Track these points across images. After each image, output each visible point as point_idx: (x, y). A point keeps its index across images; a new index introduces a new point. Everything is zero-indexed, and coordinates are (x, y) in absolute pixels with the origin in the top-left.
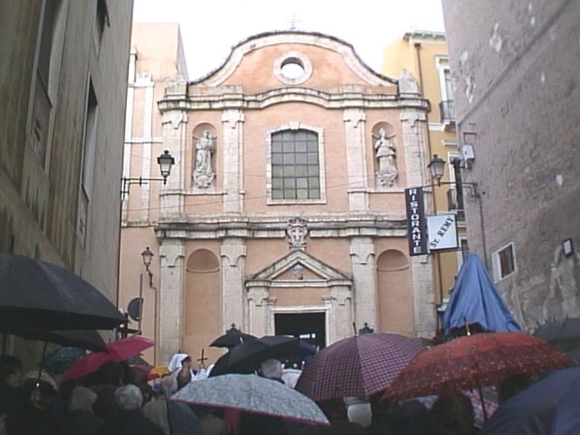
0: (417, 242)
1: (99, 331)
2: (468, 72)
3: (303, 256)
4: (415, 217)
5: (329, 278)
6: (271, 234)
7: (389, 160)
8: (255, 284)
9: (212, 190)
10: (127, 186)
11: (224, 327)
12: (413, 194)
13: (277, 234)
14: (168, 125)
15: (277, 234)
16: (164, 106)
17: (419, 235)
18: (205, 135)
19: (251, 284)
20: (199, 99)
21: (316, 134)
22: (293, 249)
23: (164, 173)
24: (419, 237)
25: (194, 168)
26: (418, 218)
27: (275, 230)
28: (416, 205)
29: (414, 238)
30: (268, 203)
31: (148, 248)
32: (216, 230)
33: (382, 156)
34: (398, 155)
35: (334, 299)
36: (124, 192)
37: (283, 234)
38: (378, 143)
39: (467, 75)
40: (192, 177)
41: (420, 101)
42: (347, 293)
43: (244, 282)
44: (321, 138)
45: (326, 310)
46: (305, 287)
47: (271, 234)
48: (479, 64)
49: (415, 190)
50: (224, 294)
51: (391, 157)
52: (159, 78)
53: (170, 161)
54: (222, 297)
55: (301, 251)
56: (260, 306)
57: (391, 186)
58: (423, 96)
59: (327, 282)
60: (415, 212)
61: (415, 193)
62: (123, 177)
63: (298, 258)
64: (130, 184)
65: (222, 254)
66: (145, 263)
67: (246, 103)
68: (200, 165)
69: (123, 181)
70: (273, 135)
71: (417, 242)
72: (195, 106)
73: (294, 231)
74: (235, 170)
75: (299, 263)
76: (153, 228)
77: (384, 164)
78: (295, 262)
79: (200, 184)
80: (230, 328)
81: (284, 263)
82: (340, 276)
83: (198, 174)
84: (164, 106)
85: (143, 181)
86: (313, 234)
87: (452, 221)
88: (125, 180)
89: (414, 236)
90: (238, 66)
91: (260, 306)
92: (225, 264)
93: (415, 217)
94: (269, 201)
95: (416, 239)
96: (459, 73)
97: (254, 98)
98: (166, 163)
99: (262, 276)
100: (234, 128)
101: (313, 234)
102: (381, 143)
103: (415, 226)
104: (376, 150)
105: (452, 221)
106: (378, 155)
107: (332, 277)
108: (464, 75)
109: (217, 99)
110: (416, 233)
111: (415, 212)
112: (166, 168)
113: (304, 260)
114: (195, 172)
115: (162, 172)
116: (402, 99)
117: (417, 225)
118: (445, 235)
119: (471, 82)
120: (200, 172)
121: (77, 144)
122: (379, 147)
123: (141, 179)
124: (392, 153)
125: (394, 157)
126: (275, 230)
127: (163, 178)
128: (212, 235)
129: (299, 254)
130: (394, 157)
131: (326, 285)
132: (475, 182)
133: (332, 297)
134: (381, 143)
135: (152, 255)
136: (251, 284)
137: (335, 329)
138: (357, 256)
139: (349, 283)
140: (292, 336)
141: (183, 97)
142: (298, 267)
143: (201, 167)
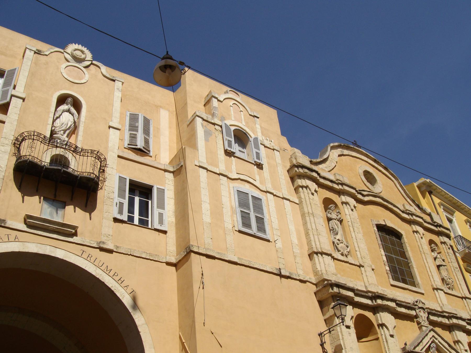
128: (368, 302)
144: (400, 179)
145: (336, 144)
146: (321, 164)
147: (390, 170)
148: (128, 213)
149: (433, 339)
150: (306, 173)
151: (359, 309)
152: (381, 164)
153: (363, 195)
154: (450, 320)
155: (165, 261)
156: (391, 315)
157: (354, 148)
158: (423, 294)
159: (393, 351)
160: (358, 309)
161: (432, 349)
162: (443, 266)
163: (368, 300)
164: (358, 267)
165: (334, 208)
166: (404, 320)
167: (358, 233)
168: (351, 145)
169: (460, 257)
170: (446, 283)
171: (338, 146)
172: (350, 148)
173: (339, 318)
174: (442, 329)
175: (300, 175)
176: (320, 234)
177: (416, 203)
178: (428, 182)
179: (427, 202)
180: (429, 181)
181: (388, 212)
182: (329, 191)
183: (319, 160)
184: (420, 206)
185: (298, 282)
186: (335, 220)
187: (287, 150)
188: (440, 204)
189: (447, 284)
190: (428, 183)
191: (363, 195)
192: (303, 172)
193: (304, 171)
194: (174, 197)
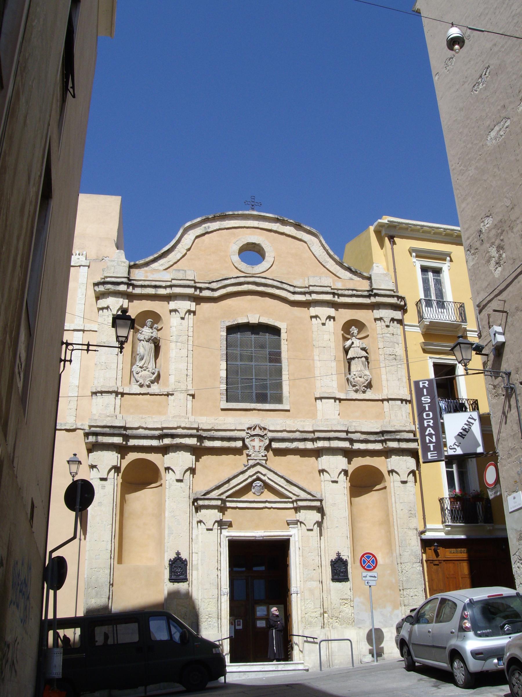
0: (431, 445)
1: (189, 471)
2: (493, 240)
3: (264, 471)
4: (428, 415)
5: (294, 498)
9: (155, 388)
10: (69, 352)
12: (424, 387)
16: (101, 288)
17: (434, 437)
20: (143, 283)
22: (251, 463)
23: (121, 339)
24: (434, 440)
25: (132, 364)
27: (230, 439)
29: (428, 441)
31: (75, 455)
33: (353, 358)
34: (372, 358)
36: (65, 361)
37: (239, 444)
38: (348, 343)
39: (493, 243)
40: (131, 372)
41: (396, 298)
43: (192, 500)
44: (283, 335)
45: (291, 536)
46: (266, 508)
47: (226, 444)
48: (511, 228)
49: (427, 383)
50: (167, 514)
51: (364, 359)
52: (95, 257)
53: (129, 322)
56: (211, 530)
57: (364, 392)
59: (292, 502)
60: (427, 409)
61: (426, 385)
62: (65, 341)
63: (258, 472)
64: (73, 350)
67: (198, 290)
68: (142, 359)
69: (64, 346)
70: (231, 330)
71: (431, 445)
72: (138, 291)
74: (183, 366)
75: (258, 479)
76: (81, 432)
78: (255, 477)
79: (141, 381)
80: (173, 556)
81: (241, 478)
82: (309, 497)
84: (101, 288)
86: (275, 445)
87: (475, 420)
88: (68, 344)
89: (427, 438)
90: (189, 250)
91: (211, 530)
92: (168, 478)
93: (428, 415)
94: (224, 405)
95: (431, 442)
96: (478, 244)
97: (207, 285)
98: (123, 326)
99: (214, 494)
100: (183, 318)
101: (275, 445)
102: (353, 343)
103: (429, 426)
104: (346, 351)
105: (475, 420)
106: (348, 357)
107: (298, 496)
108: (487, 245)
109: (164, 284)
110: (430, 435)
111: (427, 409)
112: (123, 332)
113: (264, 475)
114: (135, 366)
115: (117, 337)
116: (376, 295)
118: (465, 439)
119: (498, 251)
120: (141, 367)
121: (28, 219)
122: (350, 347)
123: (88, 350)
124: (364, 353)
125: (367, 358)
126: (230, 439)
127: (117, 344)
128: (155, 443)
130: (367, 358)
131: (290, 505)
132: (508, 371)
133: (298, 521)
134: (353, 343)
135: (80, 463)
136: (201, 503)
139: (318, 504)
142: (258, 483)
143: (143, 362)
144: (322, 235)
145: (199, 219)
146: (157, 262)
147: (304, 227)
149: (430, 431)
151: (139, 453)
152: (288, 222)
153: (213, 290)
154: (315, 443)
157: (234, 214)
159: (174, 499)
160: (138, 453)
161: (254, 488)
162: (356, 359)
163: (154, 440)
164: (166, 396)
165: (149, 323)
166: (221, 455)
168: (227, 211)
169: (421, 332)
170: (351, 384)
171: (204, 221)
172: (227, 216)
173: (461, 364)
175: (105, 293)
176: (107, 368)
177: (345, 266)
179: (384, 253)
180: (388, 221)
181: (267, 300)
182: (151, 301)
183: (142, 262)
184: (352, 268)
185: (64, 431)
186: (144, 341)
187: (108, 257)
188: (411, 251)
189: (354, 386)
191: (213, 290)
194: (66, 313)
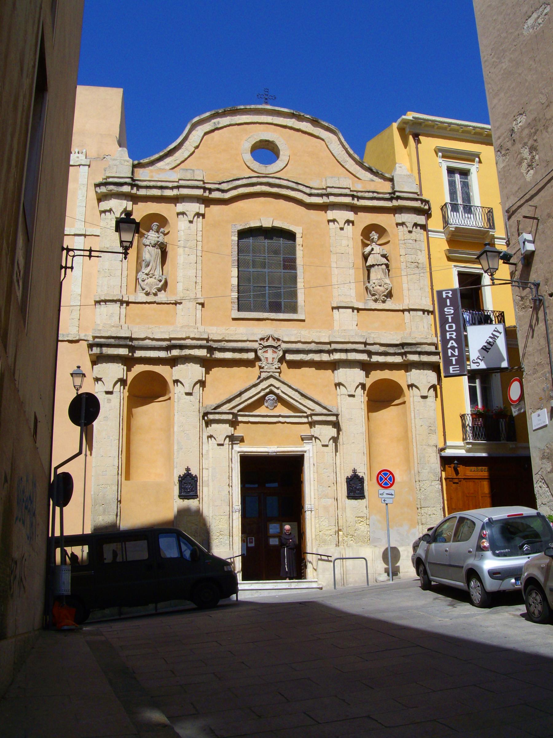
0: (454, 359)
3: (277, 384)
4: (451, 327)
5: (309, 412)
6: (237, 356)
7: (382, 269)
8: (217, 417)
9: (162, 297)
10: (70, 259)
11: (175, 470)
13: (245, 356)
14: (107, 214)
15: (245, 356)
16: (103, 189)
17: (456, 350)
18: (155, 228)
19: (211, 417)
21: (290, 236)
24: (456, 354)
26: (454, 328)
28: (452, 311)
30: (234, 316)
31: (79, 367)
32: (168, 348)
33: (373, 266)
34: (392, 266)
35: (316, 438)
36: (66, 268)
37: (251, 355)
38: (368, 249)
39: (525, 144)
40: (137, 279)
41: (419, 202)
42: (333, 432)
43: (202, 414)
44: (299, 240)
45: (305, 452)
46: (280, 422)
47: (237, 356)
49: (451, 293)
51: (384, 267)
54: (174, 432)
55: (275, 378)
56: (222, 445)
57: (384, 302)
58: (422, 195)
59: (307, 417)
60: (450, 320)
61: (450, 295)
63: (271, 385)
64: (74, 256)
65: (174, 378)
66: (75, 386)
67: (207, 192)
70: (243, 234)
72: (142, 192)
73: (266, 352)
75: (271, 392)
76: (85, 343)
77: (376, 274)
78: (268, 390)
79: (147, 289)
80: (183, 472)
82: (325, 411)
83: (145, 277)
84: (103, 189)
85: (87, 253)
86: (289, 357)
87: (500, 333)
88: (68, 250)
89: (450, 351)
90: (197, 147)
91: (222, 445)
92: (177, 392)
93: (451, 327)
94: (236, 314)
95: (453, 355)
96: (509, 144)
97: (217, 186)
100: (191, 222)
101: (289, 357)
103: (451, 338)
104: (366, 258)
105: (500, 333)
106: (368, 264)
108: (519, 146)
109: (170, 185)
110: (453, 348)
111: (450, 320)
112: (127, 237)
113: (278, 388)
115: (121, 242)
116: (398, 198)
117: (454, 336)
120: (147, 274)
123: (90, 256)
124: (384, 261)
125: (387, 266)
127: (121, 250)
128: (162, 354)
129: (272, 381)
130: (387, 266)
131: (305, 420)
132: (537, 282)
133: (313, 436)
134: (372, 249)
135: (84, 375)
136: (211, 417)
137: (316, 476)
138: (343, 385)
139: (333, 418)
140: (276, 485)
141: (128, 180)
145: (208, 114)
148: (182, 497)
150: (111, 191)
153: (223, 191)
155: (73, 266)
156: (314, 369)
157: (246, 108)
158: (304, 321)
162: (376, 266)
163: (161, 352)
165: (155, 227)
167: (189, 255)
169: (446, 239)
170: (370, 293)
174: (316, 369)
176: (111, 275)
177: (365, 166)
178: (412, 119)
180: (413, 118)
181: (282, 202)
183: (146, 160)
186: (149, 246)
188: (437, 151)
190: (411, 120)
191: (223, 191)
192: (107, 190)
193: (108, 189)
